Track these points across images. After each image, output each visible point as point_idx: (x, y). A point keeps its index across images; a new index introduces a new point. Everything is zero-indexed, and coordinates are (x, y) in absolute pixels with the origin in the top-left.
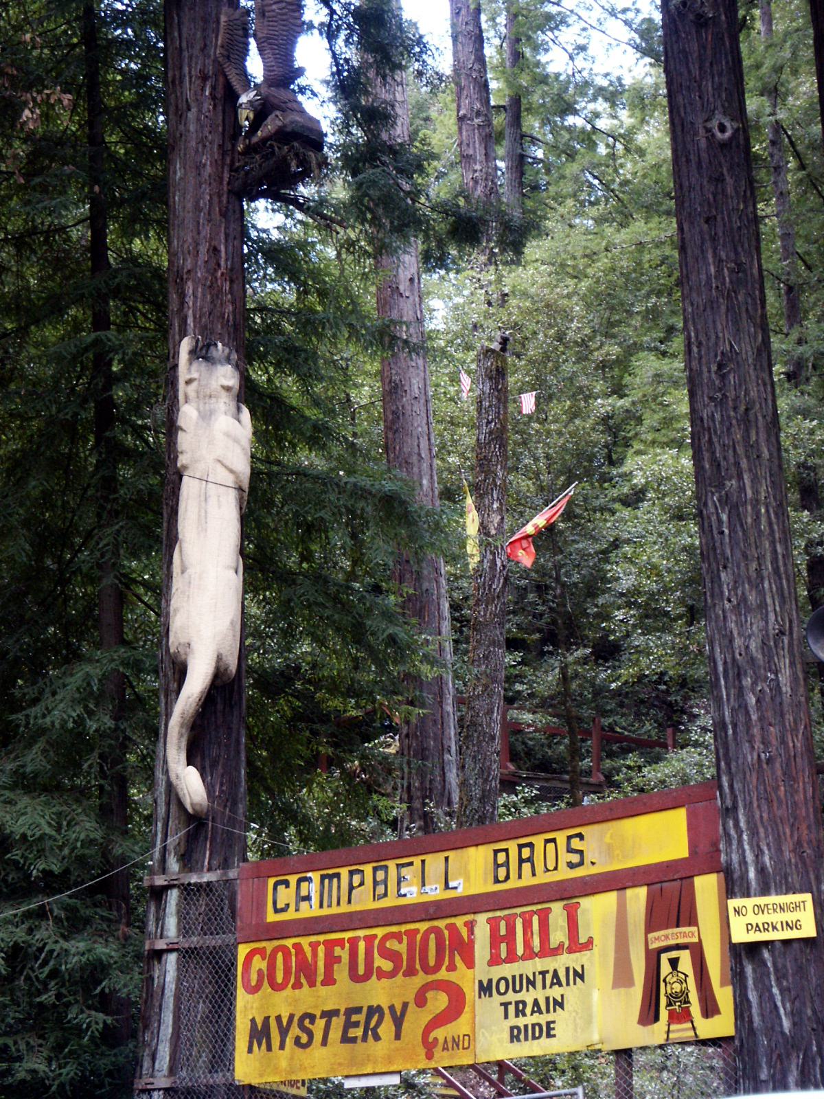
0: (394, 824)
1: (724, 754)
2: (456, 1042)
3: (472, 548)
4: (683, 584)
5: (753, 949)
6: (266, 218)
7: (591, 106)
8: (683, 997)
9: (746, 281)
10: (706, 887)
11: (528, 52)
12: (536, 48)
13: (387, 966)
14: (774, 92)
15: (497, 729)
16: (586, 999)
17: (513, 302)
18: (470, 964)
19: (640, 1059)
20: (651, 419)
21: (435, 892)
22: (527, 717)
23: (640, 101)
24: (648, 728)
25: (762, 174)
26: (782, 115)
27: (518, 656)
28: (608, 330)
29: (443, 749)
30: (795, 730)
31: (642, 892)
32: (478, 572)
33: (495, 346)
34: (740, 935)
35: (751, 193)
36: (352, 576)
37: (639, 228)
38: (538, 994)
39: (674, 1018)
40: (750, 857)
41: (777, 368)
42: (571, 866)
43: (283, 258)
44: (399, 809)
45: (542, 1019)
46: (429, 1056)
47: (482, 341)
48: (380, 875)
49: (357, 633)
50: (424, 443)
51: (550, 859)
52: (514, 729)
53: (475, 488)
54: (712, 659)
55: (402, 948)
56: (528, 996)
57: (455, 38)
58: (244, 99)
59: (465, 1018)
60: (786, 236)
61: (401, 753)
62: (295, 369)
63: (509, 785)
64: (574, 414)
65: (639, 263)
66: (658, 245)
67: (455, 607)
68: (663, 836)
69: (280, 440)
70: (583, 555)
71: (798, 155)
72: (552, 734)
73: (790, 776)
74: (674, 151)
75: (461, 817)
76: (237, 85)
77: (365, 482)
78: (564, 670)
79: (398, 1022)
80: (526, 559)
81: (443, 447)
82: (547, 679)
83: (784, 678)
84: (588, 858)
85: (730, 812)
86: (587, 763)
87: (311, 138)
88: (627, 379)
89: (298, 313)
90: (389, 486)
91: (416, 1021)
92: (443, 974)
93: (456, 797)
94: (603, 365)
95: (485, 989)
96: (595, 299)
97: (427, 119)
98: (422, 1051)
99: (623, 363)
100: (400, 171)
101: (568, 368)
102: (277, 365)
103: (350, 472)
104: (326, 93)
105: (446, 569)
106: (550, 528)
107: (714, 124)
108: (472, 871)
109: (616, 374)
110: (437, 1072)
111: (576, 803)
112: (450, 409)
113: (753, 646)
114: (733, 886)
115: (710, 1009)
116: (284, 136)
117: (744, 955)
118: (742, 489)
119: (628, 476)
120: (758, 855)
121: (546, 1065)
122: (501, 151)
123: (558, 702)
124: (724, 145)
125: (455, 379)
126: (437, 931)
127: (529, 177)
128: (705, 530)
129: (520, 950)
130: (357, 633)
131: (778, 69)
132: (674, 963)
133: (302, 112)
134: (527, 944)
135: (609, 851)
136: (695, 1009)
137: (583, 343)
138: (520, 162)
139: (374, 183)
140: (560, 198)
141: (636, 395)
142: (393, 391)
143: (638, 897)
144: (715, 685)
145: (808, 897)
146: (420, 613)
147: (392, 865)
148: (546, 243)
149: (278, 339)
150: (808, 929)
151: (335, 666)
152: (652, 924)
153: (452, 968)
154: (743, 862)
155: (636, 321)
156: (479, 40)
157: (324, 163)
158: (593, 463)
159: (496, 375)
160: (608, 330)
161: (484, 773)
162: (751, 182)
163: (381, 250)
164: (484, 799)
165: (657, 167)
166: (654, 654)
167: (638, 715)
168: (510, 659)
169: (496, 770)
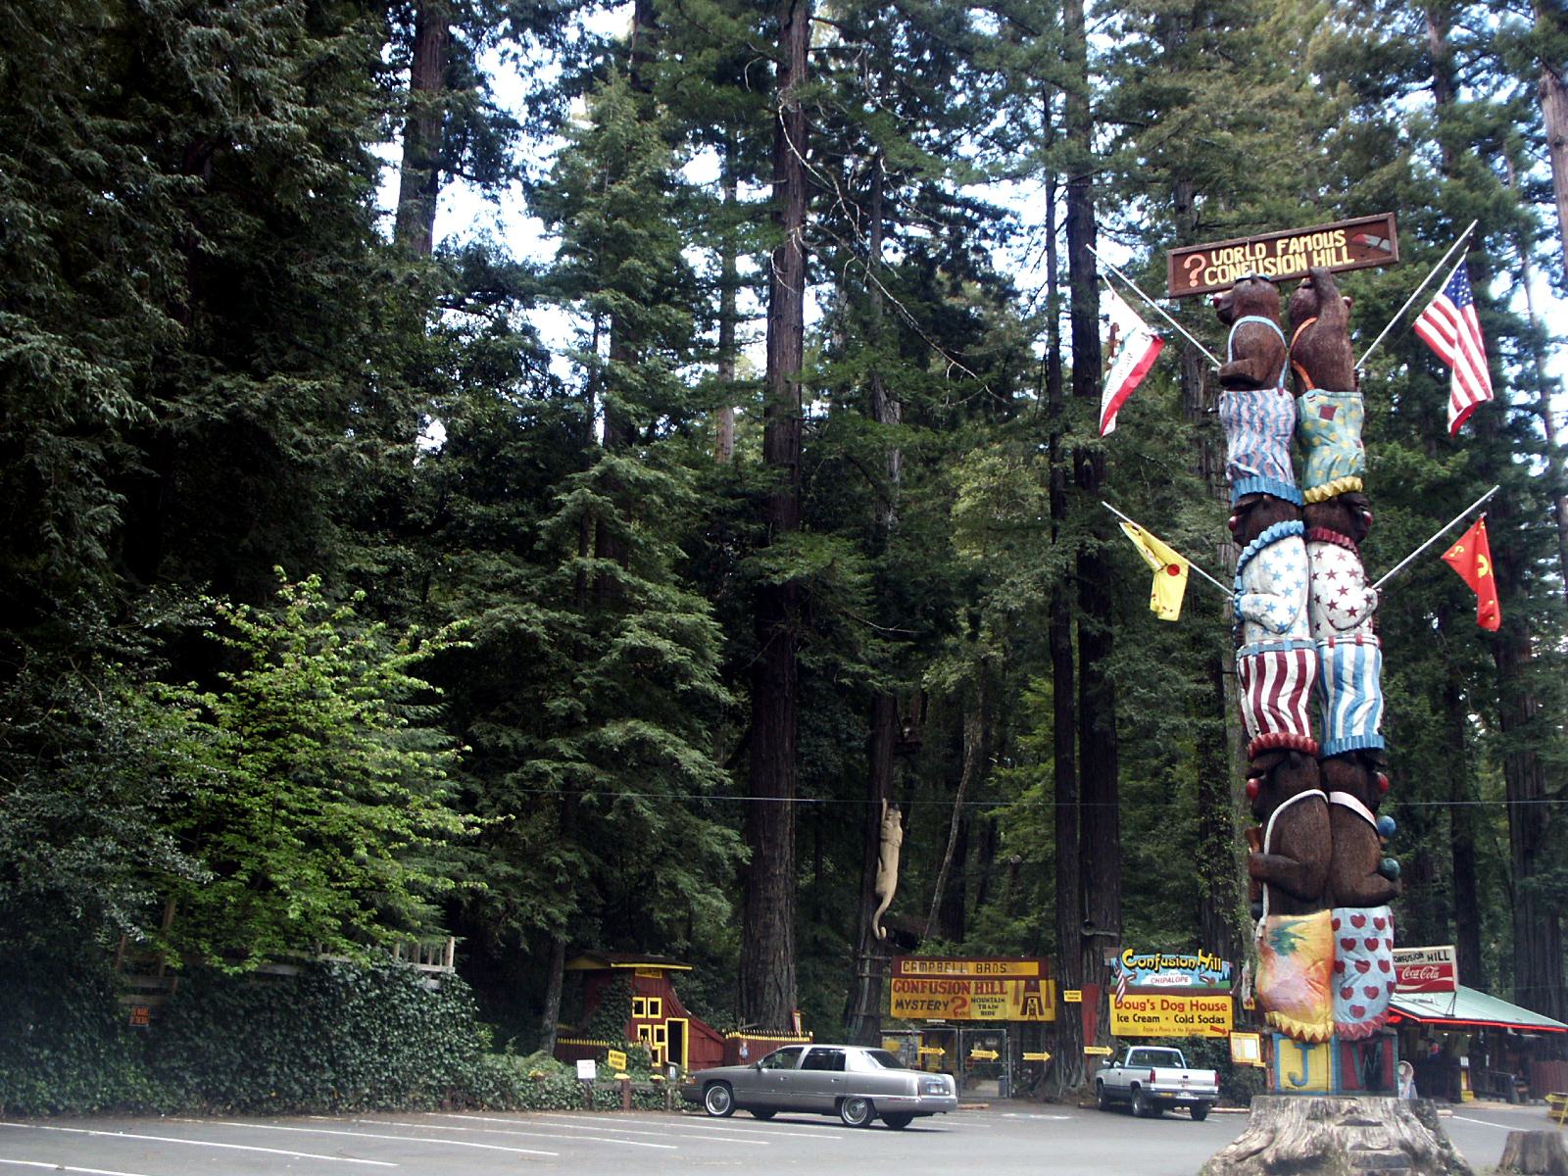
21: (957, 973)
51: (995, 969)
91: (951, 1007)
108: (970, 969)
143: (1022, 983)
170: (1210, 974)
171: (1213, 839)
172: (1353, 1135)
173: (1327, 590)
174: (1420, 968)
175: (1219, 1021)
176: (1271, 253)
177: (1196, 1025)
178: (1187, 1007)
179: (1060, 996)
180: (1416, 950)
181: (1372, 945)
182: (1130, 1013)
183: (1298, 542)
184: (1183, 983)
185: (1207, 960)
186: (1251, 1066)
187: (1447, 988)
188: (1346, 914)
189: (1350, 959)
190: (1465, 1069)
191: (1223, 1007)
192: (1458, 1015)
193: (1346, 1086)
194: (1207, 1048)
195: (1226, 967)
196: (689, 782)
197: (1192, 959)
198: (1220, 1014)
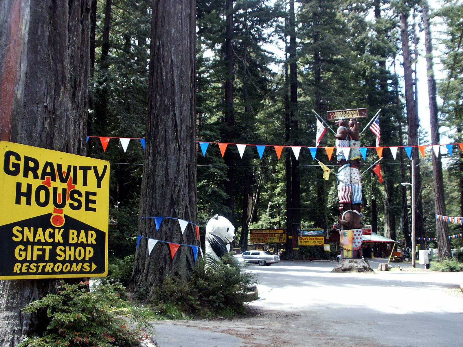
171: (320, 202)
172: (355, 265)
173: (353, 176)
176: (346, 113)
177: (317, 243)
179: (287, 237)
181: (359, 235)
182: (302, 241)
183: (349, 168)
187: (370, 234)
188: (355, 230)
189: (355, 237)
193: (354, 257)
194: (319, 248)
195: (323, 230)
196: (223, 199)
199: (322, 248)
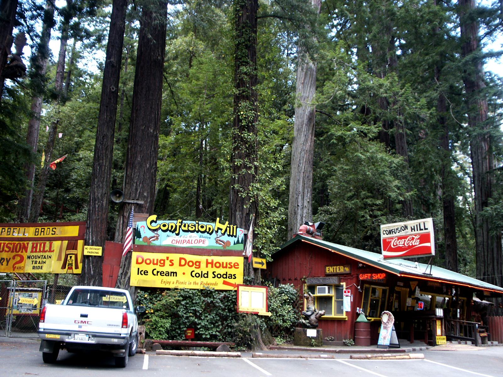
0: (14, 220)
1: (89, 216)
2: (20, 268)
3: (42, 164)
4: (86, 180)
5: (88, 257)
6: (9, 83)
7: (86, 77)
8: (71, 264)
9: (112, 121)
10: (80, 242)
11: (74, 62)
12: (77, 61)
13: (7, 250)
14: (125, 84)
15: (41, 203)
16: (51, 262)
17: (61, 113)
18: (26, 252)
19: (60, 276)
20: (86, 144)
21: (21, 235)
22: (48, 201)
23: (97, 78)
24: (73, 208)
25: (119, 99)
26: (125, 89)
27: (48, 188)
28: (80, 124)
29: (28, 205)
30: (104, 214)
31: (67, 242)
32: (43, 169)
33: (56, 122)
34: (86, 253)
35: (116, 103)
36: (14, 165)
37: (91, 104)
38: (40, 260)
39: (69, 268)
40: (91, 238)
41: (115, 139)
42: (52, 234)
43: (11, 92)
44: (15, 217)
45: (40, 265)
46: (14, 270)
47: (52, 120)
48: (9, 230)
49: (13, 177)
50: (36, 139)
51: (48, 232)
52: (44, 203)
53: (46, 151)
54: (90, 196)
55: (11, 246)
56: (38, 260)
57: (59, 55)
58: (9, 56)
59: (23, 263)
60: (121, 113)
61: (18, 204)
62: (10, 117)
63: (41, 215)
64: (70, 140)
65: (90, 111)
66: (95, 109)
67: (36, 175)
68: (73, 231)
69: (3, 132)
70: (66, 169)
71: (127, 97)
72: (52, 206)
73: (101, 223)
74: (102, 91)
75: (29, 220)
76: (8, 53)
77: (21, 145)
78: (57, 193)
79: (8, 262)
80: (54, 168)
81: (40, 141)
82: (54, 194)
83: (104, 203)
84: (56, 233)
85: (88, 228)
86: (59, 213)
87: (23, 68)
88: (83, 135)
89: (12, 105)
90: (26, 147)
91: (12, 262)
92: (20, 253)
93: (29, 216)
94: (78, 131)
95: (29, 257)
96: (78, 117)
97: (50, 70)
98: (12, 269)
99: (82, 131)
100: (42, 80)
101: (70, 130)
102: (5, 116)
103: (18, 142)
104: (28, 59)
105: (35, 167)
106: (60, 162)
107: (111, 87)
108: (30, 232)
109: (80, 133)
110: (14, 274)
111: (55, 221)
112: (43, 133)
113: (99, 195)
114: (86, 243)
115: (77, 267)
116: (17, 66)
117: (86, 258)
118: (103, 163)
119: (79, 155)
120: (92, 238)
121: (39, 275)
122: (65, 81)
123: (55, 200)
124: (113, 92)
125: (45, 127)
126: (20, 244)
127: (69, 88)
128: (94, 170)
129: (38, 250)
130: (13, 177)
131: (126, 79)
132: (71, 257)
133: (22, 62)
134: (40, 249)
135: (61, 232)
136: (74, 267)
137: (75, 126)
138: (68, 85)
139: (36, 82)
140: (76, 94)
141: (84, 139)
142: (31, 127)
143: (66, 243)
144: (90, 201)
145: (101, 248)
146: (28, 175)
147: (12, 228)
148: (71, 103)
149: (7, 110)
150: (100, 254)
151: (7, 183)
152: (68, 248)
153: (22, 252)
154: (89, 239)
155: (87, 123)
156: (64, 57)
157: (25, 74)
158: (72, 151)
159: (54, 127)
160: (80, 124)
161: (36, 212)
162: (117, 101)
163: (34, 96)
164: (35, 217)
165: (97, 93)
166: (77, 193)
167: (72, 205)
168: (46, 189)
169: (39, 212)
170: (225, 238)
174: (405, 237)
175: (231, 276)
178: (203, 265)
180: (402, 224)
182: (150, 268)
184: (201, 245)
185: (224, 227)
186: (256, 314)
190: (440, 319)
191: (236, 266)
192: (434, 276)
197: (211, 225)
198: (232, 271)
199: (231, 300)
